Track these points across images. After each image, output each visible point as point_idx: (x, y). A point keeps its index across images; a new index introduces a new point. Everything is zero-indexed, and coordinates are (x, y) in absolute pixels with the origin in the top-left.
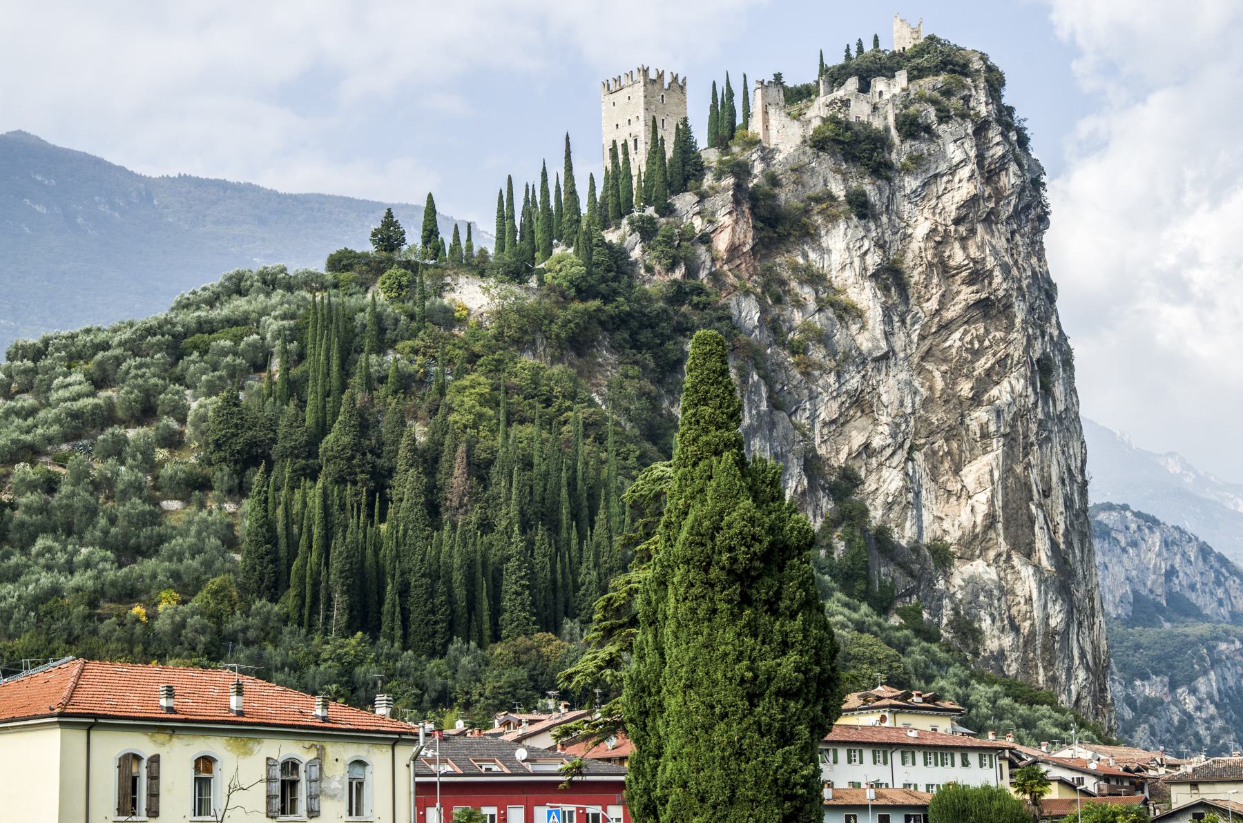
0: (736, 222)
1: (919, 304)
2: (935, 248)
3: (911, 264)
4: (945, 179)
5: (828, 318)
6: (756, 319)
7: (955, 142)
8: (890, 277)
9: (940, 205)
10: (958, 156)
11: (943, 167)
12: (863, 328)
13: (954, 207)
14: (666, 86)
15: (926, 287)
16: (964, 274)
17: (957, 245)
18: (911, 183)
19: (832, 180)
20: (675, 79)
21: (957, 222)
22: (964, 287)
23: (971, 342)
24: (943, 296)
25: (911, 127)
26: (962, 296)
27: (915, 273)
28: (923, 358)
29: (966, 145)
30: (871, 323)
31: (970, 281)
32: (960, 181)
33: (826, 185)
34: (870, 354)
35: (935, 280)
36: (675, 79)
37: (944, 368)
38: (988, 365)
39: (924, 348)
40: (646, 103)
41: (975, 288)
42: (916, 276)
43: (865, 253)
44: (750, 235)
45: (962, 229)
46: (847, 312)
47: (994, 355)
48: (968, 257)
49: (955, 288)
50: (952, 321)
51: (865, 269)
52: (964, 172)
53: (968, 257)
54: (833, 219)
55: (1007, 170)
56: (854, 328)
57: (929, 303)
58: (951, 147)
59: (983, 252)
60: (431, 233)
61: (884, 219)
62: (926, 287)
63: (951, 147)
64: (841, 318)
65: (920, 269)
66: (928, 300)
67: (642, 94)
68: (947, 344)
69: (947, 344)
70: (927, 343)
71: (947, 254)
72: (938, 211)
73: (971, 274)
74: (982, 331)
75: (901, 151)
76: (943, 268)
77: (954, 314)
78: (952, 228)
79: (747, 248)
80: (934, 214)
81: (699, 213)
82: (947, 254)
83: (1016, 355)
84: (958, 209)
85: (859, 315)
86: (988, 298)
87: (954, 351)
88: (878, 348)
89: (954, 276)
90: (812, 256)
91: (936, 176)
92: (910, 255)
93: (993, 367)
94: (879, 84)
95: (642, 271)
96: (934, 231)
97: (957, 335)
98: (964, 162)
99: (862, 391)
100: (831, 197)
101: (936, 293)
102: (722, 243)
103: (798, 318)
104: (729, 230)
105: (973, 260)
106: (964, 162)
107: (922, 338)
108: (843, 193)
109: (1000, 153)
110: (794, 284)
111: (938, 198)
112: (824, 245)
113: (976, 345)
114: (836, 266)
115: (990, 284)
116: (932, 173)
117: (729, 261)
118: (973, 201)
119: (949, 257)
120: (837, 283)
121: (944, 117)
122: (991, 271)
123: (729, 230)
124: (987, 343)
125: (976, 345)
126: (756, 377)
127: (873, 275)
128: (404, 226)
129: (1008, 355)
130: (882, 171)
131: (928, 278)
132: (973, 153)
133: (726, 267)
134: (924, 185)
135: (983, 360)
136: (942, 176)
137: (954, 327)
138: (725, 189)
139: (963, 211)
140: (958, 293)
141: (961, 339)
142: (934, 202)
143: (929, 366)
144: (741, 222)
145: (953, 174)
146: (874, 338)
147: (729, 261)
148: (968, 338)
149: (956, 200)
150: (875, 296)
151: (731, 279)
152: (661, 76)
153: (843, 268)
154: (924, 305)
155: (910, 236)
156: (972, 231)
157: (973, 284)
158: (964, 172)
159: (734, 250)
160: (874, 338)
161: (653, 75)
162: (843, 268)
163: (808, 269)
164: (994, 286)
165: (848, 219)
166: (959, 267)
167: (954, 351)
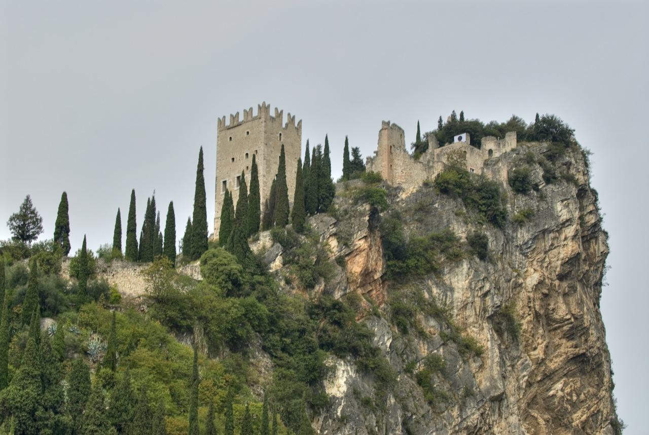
0: (370, 247)
1: (527, 351)
2: (542, 300)
3: (521, 312)
4: (552, 235)
5: (450, 353)
6: (388, 344)
7: (562, 201)
8: (503, 322)
9: (547, 260)
10: (564, 215)
11: (550, 224)
12: (482, 367)
13: (559, 262)
14: (284, 126)
15: (533, 336)
16: (566, 328)
17: (561, 299)
18: (523, 235)
19: (454, 222)
20: (292, 120)
21: (561, 277)
22: (564, 341)
23: (570, 394)
24: (547, 347)
25: (520, 184)
26: (562, 350)
27: (524, 321)
28: (529, 405)
29: (571, 206)
30: (489, 362)
31: (569, 336)
32: (566, 239)
33: (448, 226)
34: (488, 391)
35: (541, 331)
36: (292, 120)
37: (547, 416)
38: (584, 417)
39: (530, 395)
40: (266, 138)
41: (574, 342)
42: (525, 324)
43: (485, 295)
44: (380, 263)
45: (565, 284)
46: (470, 350)
47: (588, 408)
48: (570, 312)
49: (556, 341)
50: (554, 372)
51: (485, 310)
52: (570, 231)
53: (570, 312)
54: (455, 259)
55: (596, 238)
56: (474, 366)
57: (536, 352)
58: (559, 207)
59: (582, 309)
60: (62, 228)
61: (500, 265)
62: (533, 336)
63: (559, 207)
64: (462, 353)
65: (528, 318)
66: (535, 349)
67: (262, 129)
68: (551, 393)
69: (551, 393)
70: (534, 390)
71: (552, 307)
72: (545, 265)
73: (572, 328)
74: (578, 384)
75: (515, 205)
76: (545, 319)
77: (556, 365)
78: (557, 283)
79: (377, 276)
80: (542, 267)
81: (335, 235)
82: (552, 307)
83: (605, 411)
84: (562, 265)
85: (479, 353)
86: (584, 354)
87: (556, 400)
88: (496, 387)
89: (555, 329)
90: (435, 291)
91: (544, 232)
92: (520, 304)
93: (586, 421)
94: (489, 144)
95: (282, 283)
96: (541, 283)
97: (559, 386)
98: (569, 222)
99: (481, 428)
100: (450, 238)
101: (541, 344)
102: (356, 266)
103: (424, 350)
104: (365, 257)
105: (573, 315)
106: (569, 222)
107: (529, 384)
108: (464, 235)
109: (593, 221)
110: (420, 316)
111: (546, 252)
112: (448, 282)
113: (575, 398)
114: (458, 304)
115: (586, 341)
116: (541, 229)
117: (362, 285)
118: (573, 260)
119: (553, 310)
120: (457, 320)
121: (549, 178)
122: (588, 329)
123: (364, 254)
124: (582, 397)
125: (575, 398)
126: (393, 401)
127: (489, 318)
128: (41, 213)
129: (599, 411)
130: (497, 219)
131: (535, 328)
132: (577, 214)
133: (359, 291)
134: (534, 239)
135: (579, 413)
136: (550, 232)
137: (556, 378)
138: (362, 214)
139: (567, 268)
140: (559, 346)
141: (562, 390)
142: (542, 255)
143: (535, 413)
144: (373, 249)
145: (559, 231)
146: (492, 378)
147: (362, 285)
148: (568, 390)
149: (561, 256)
150: (492, 338)
151: (364, 303)
152: (280, 115)
153: (465, 307)
154: (532, 353)
155: (520, 285)
156: (573, 289)
157: (573, 339)
158: (570, 231)
159: (367, 274)
160: (492, 378)
161: (272, 113)
162: (465, 307)
163: (432, 304)
164: (589, 344)
165: (471, 260)
166: (563, 321)
167: (556, 400)
